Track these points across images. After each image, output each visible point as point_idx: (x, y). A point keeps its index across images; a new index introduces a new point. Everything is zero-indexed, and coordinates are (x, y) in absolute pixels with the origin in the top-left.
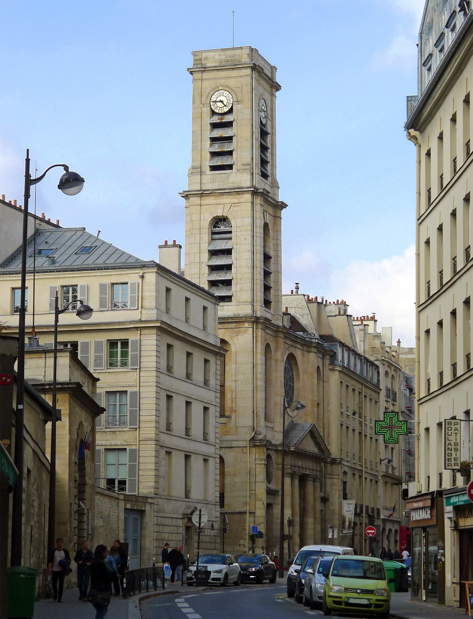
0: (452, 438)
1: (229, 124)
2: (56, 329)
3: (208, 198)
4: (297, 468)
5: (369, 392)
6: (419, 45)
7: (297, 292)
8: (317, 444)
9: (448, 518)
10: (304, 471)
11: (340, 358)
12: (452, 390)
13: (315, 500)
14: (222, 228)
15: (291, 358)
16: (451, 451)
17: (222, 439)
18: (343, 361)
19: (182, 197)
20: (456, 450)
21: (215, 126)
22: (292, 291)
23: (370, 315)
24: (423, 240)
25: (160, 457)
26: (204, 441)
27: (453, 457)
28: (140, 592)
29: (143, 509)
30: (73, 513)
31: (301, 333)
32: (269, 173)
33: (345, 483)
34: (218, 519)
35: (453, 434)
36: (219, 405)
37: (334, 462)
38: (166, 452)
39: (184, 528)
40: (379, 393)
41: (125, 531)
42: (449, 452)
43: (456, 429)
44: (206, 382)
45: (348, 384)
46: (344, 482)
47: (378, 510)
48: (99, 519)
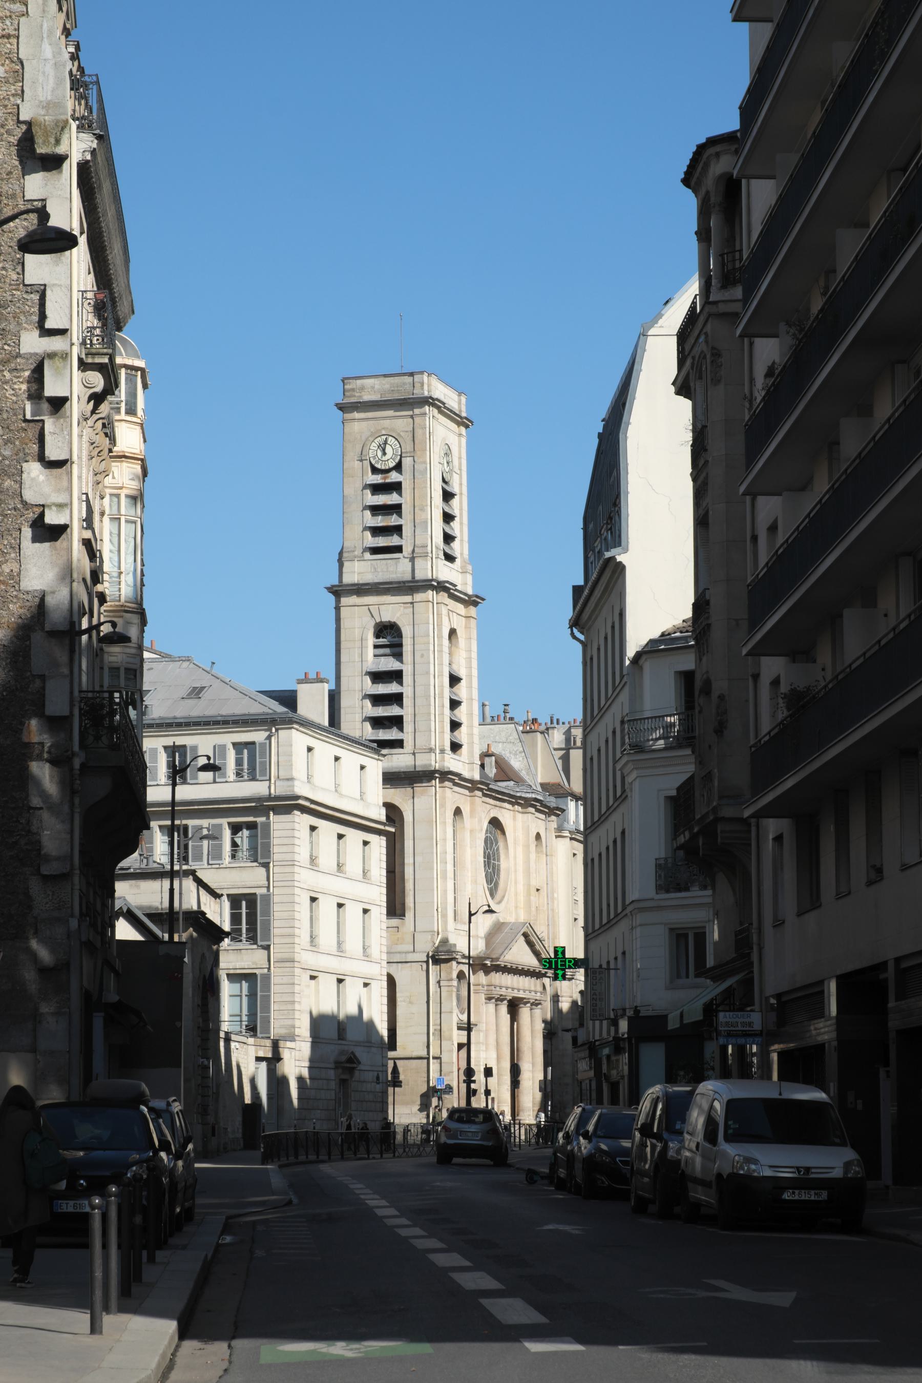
1: (396, 487)
2: (173, 809)
15: (495, 823)
17: (393, 950)
21: (377, 489)
26: (366, 959)
28: (279, 1160)
31: (512, 783)
36: (385, 904)
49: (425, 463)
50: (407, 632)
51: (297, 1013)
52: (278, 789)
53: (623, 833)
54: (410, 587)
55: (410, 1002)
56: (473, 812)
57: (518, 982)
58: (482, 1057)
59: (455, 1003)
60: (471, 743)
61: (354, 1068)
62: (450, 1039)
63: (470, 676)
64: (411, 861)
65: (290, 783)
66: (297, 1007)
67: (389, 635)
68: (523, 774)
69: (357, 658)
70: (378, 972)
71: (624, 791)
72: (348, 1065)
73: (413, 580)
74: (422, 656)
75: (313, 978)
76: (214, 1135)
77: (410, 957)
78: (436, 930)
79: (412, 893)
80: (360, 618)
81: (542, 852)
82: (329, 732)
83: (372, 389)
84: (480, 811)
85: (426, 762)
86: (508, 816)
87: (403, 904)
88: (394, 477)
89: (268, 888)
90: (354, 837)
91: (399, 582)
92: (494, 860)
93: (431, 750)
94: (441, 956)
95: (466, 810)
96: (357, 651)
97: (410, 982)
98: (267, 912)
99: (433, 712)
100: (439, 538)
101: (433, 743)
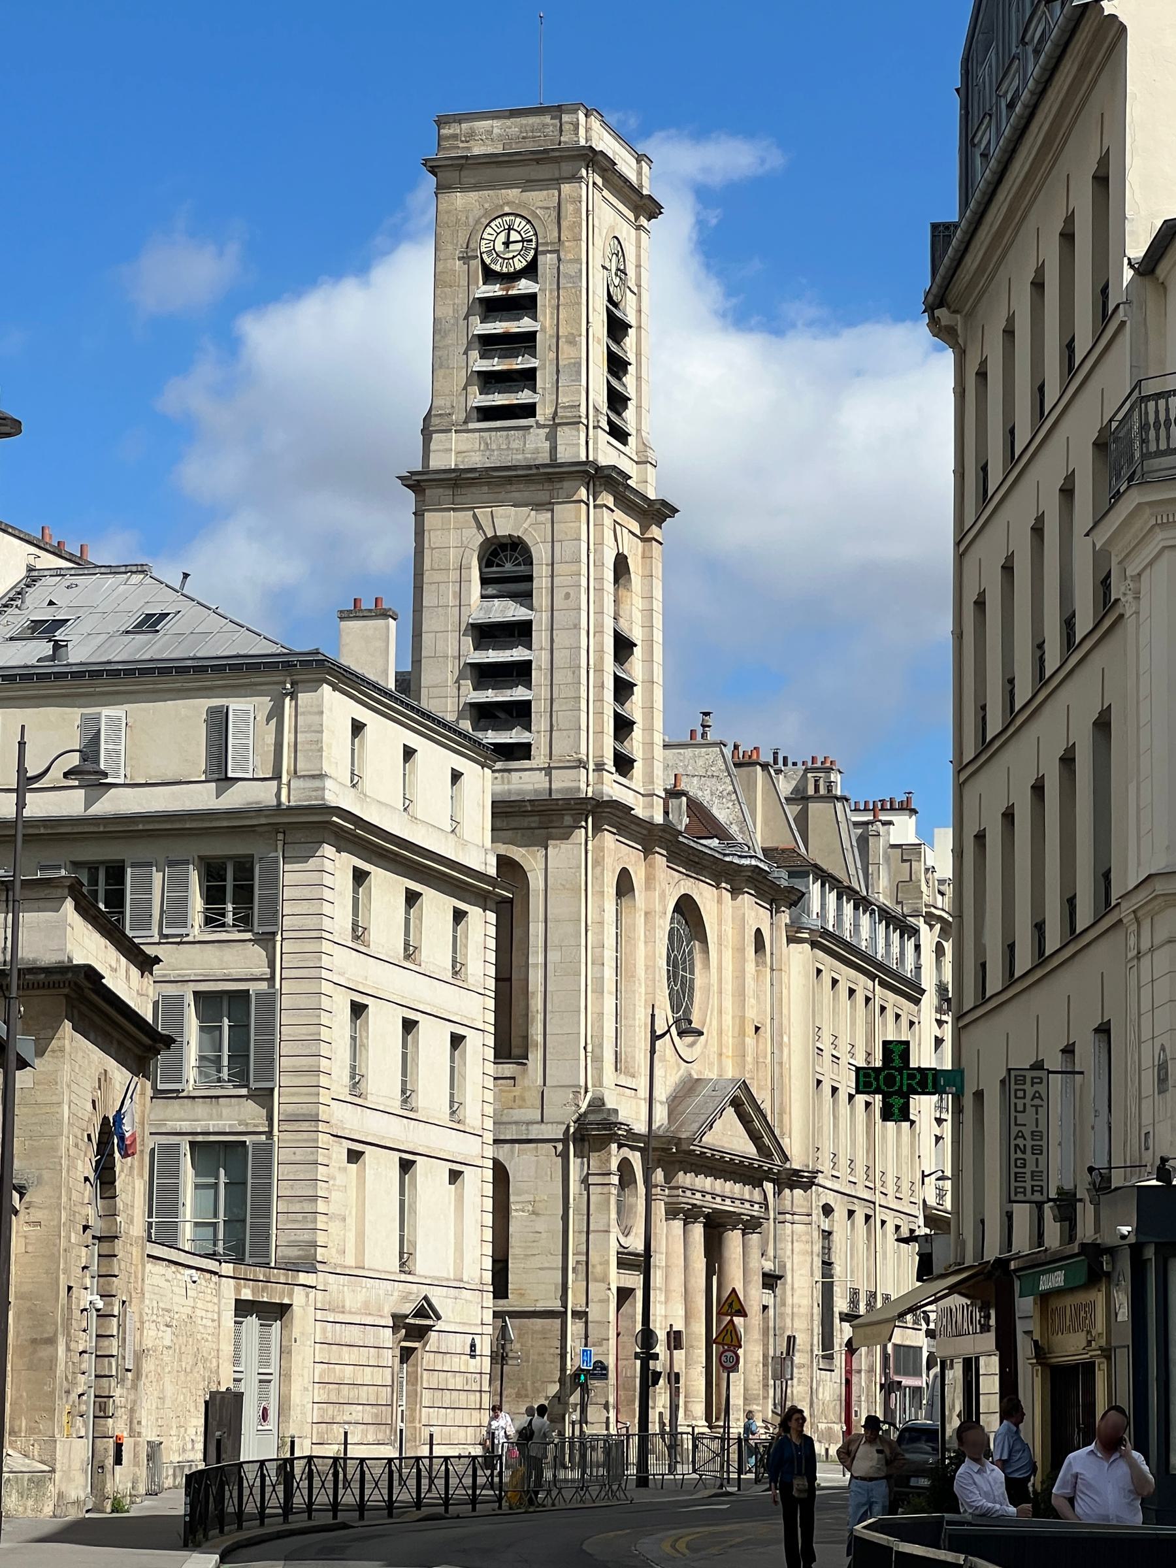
0: (1027, 1118)
1: (527, 304)
3: (473, 489)
6: (963, 92)
7: (704, 735)
8: (755, 1137)
9: (1025, 1332)
10: (718, 1204)
11: (815, 907)
12: (1034, 992)
14: (508, 566)
15: (686, 908)
16: (1024, 1152)
17: (505, 1119)
18: (822, 915)
19: (408, 486)
20: (1038, 1151)
21: (492, 308)
23: (900, 797)
24: (970, 597)
27: (1028, 1170)
29: (286, 1301)
30: (425, 1291)
31: (714, 843)
32: (631, 428)
33: (827, 1235)
34: (489, 1330)
35: (1028, 1106)
36: (492, 1029)
37: (801, 1180)
38: (350, 1152)
39: (398, 1352)
40: (917, 1002)
41: (236, 1360)
42: (1019, 1155)
43: (1037, 1096)
44: (457, 968)
45: (837, 977)
48: (163, 1328)
49: (579, 261)
50: (540, 553)
51: (321, 1222)
52: (294, 794)
53: (1103, 725)
54: (549, 481)
56: (650, 880)
58: (668, 1313)
60: (649, 760)
61: (429, 1328)
62: (605, 1279)
63: (650, 642)
64: (541, 960)
65: (316, 783)
66: (321, 1206)
67: (506, 564)
68: (734, 830)
70: (476, 1151)
71: (1105, 601)
72: (418, 1321)
73: (553, 463)
75: (354, 1156)
76: (118, 1461)
77: (535, 1132)
78: (582, 1083)
79: (540, 1017)
80: (457, 537)
82: (396, 700)
83: (488, 137)
84: (662, 884)
86: (707, 896)
87: (526, 1037)
88: (524, 286)
89: (272, 979)
90: (437, 905)
91: (529, 467)
92: (684, 970)
93: (581, 764)
94: (593, 1132)
95: (638, 879)
96: (452, 588)
97: (534, 1173)
98: (268, 1026)
99: (584, 695)
100: (600, 397)
101: (583, 750)
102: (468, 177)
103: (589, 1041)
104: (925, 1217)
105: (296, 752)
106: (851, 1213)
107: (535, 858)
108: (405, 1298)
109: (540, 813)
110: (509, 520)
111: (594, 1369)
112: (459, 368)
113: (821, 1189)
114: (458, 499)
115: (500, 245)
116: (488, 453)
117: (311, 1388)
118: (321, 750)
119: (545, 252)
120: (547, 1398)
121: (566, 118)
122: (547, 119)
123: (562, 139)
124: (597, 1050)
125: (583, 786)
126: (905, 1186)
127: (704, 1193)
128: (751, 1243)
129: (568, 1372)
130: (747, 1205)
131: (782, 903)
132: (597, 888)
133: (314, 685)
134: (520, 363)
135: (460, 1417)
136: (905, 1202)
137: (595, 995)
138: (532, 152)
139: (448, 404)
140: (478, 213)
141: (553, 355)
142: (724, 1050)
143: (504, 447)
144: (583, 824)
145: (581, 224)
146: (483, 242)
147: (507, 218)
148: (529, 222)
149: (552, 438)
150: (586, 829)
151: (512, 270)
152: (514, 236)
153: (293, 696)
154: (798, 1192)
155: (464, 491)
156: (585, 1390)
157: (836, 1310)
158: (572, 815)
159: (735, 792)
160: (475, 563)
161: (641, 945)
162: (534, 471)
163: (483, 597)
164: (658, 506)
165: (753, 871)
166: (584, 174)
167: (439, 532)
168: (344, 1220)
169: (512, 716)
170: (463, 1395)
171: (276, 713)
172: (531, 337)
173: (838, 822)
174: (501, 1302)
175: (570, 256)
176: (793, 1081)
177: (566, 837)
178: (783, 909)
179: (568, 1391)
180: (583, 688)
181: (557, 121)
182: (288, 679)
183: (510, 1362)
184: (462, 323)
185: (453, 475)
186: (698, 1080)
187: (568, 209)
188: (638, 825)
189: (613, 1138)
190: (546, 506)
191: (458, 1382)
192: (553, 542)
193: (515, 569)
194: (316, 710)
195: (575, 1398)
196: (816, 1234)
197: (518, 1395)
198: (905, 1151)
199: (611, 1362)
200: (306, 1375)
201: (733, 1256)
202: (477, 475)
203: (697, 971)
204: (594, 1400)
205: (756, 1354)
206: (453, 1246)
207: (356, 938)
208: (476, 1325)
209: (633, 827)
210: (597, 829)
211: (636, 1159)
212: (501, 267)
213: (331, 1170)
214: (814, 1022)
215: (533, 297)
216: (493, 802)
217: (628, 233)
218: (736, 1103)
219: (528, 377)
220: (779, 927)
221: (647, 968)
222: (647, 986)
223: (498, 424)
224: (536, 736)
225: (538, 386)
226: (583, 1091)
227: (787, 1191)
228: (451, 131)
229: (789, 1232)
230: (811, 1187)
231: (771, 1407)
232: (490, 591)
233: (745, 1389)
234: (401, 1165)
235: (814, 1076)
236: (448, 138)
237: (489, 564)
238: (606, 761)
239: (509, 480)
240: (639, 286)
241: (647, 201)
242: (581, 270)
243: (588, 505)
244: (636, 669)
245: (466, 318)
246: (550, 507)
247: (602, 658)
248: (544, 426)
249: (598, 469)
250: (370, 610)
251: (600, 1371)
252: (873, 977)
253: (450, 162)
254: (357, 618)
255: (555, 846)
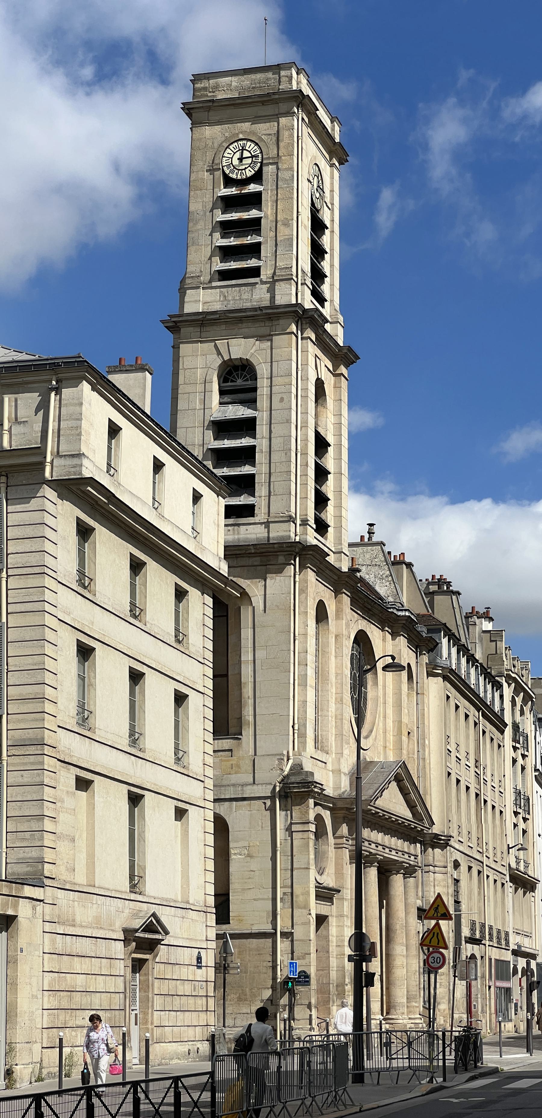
3: (215, 328)
4: (373, 846)
5: (489, 727)
7: (370, 538)
8: (411, 806)
10: (388, 854)
11: (445, 654)
13: (407, 913)
14: (239, 382)
15: (362, 640)
21: (229, 203)
22: (362, 537)
25: (60, 787)
29: (10, 912)
30: (154, 909)
33: (457, 881)
34: (213, 945)
39: (129, 963)
40: (502, 732)
46: (455, 879)
47: (507, 934)
49: (292, 169)
50: (262, 370)
51: (48, 840)
54: (268, 320)
55: (249, 856)
57: (390, 841)
59: (312, 856)
61: (158, 942)
62: (306, 906)
65: (75, 461)
66: (48, 825)
67: (238, 380)
69: (198, 405)
73: (273, 306)
74: (282, 400)
75: (83, 784)
80: (201, 362)
81: (412, 688)
85: (281, 534)
88: (253, 188)
91: (255, 309)
93: (291, 519)
94: (295, 790)
96: (198, 397)
97: (248, 824)
99: (293, 470)
101: (293, 509)
102: (214, 116)
103: (296, 722)
104: (510, 875)
105: (59, 437)
106: (470, 868)
107: (257, 588)
108: (135, 915)
109: (261, 554)
110: (240, 348)
111: (299, 977)
112: (206, 245)
113: (452, 849)
114: (204, 334)
115: (236, 161)
116: (225, 303)
117: (40, 996)
118: (80, 434)
119: (268, 164)
120: (262, 1001)
121: (283, 73)
122: (270, 75)
123: (281, 87)
124: (302, 728)
125: (293, 535)
126: (499, 854)
127: (377, 844)
128: (409, 884)
129: (279, 980)
130: (406, 856)
131: (424, 648)
132: (302, 609)
133: (75, 382)
134: (250, 240)
135: (189, 1018)
136: (499, 864)
137: (301, 688)
138: (259, 96)
139: (198, 270)
140: (220, 139)
141: (273, 234)
142: (388, 744)
143: (238, 298)
144: (293, 562)
145: (293, 144)
146: (224, 159)
147: (241, 143)
148: (257, 144)
149: (272, 291)
150: (295, 566)
151: (244, 177)
152: (246, 154)
153: (58, 391)
154: (437, 851)
155: (208, 329)
156: (292, 994)
157: (463, 935)
158: (285, 556)
159: (391, 575)
160: (215, 379)
161: (333, 658)
162: (259, 312)
163: (220, 403)
164: (345, 351)
165: (406, 620)
166: (296, 111)
167: (190, 358)
168: (73, 840)
169: (241, 487)
170: (191, 1000)
171: (44, 406)
172: (257, 222)
173: (454, 608)
174: (224, 927)
175: (285, 166)
176: (432, 770)
177: (280, 571)
178: (424, 652)
179: (279, 995)
180: (293, 466)
181: (277, 76)
182: (54, 377)
183: (231, 972)
184: (209, 214)
185: (201, 317)
186: (371, 762)
187: (285, 134)
188: (331, 570)
189: (310, 794)
190: (268, 337)
191: (187, 989)
192: (272, 362)
193: (245, 383)
194: (76, 401)
195: (284, 1000)
196: (450, 881)
197: (240, 999)
198: (498, 830)
199: (312, 972)
200: (34, 984)
201: (398, 893)
202: (218, 316)
203: (369, 687)
204: (299, 1002)
205: (414, 965)
206: (180, 874)
207: (81, 583)
208: (202, 940)
209: (327, 571)
210: (302, 567)
211: (327, 815)
212: (237, 175)
213: (58, 793)
214: (445, 733)
215: (259, 194)
216: (225, 547)
217: (325, 167)
218: (398, 779)
219: (255, 250)
220: (421, 665)
221: (337, 674)
222: (337, 688)
223: (234, 282)
224: (259, 499)
225: (262, 255)
226: (285, 760)
227: (430, 850)
228: (202, 85)
229: (432, 879)
230: (446, 847)
231: (422, 1003)
232: (226, 399)
233: (407, 992)
234: (130, 798)
235: (446, 769)
236: (200, 89)
237: (226, 380)
238: (309, 518)
239: (240, 320)
240: (332, 204)
241: (337, 147)
242: (293, 176)
243: (297, 337)
244: (329, 462)
245: (212, 211)
246: (270, 338)
247: (306, 445)
248: (266, 283)
249: (305, 311)
250: (131, 366)
251: (304, 978)
252: (478, 709)
253: (201, 105)
254: (121, 371)
255: (272, 578)
